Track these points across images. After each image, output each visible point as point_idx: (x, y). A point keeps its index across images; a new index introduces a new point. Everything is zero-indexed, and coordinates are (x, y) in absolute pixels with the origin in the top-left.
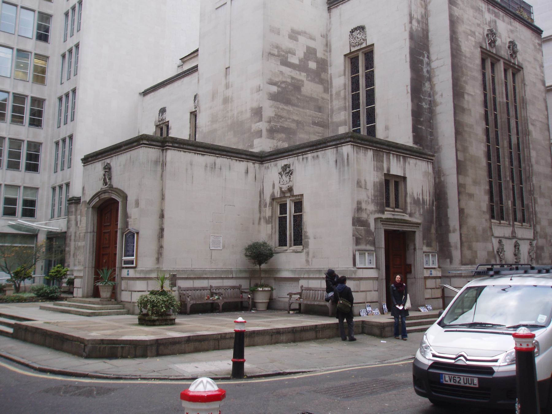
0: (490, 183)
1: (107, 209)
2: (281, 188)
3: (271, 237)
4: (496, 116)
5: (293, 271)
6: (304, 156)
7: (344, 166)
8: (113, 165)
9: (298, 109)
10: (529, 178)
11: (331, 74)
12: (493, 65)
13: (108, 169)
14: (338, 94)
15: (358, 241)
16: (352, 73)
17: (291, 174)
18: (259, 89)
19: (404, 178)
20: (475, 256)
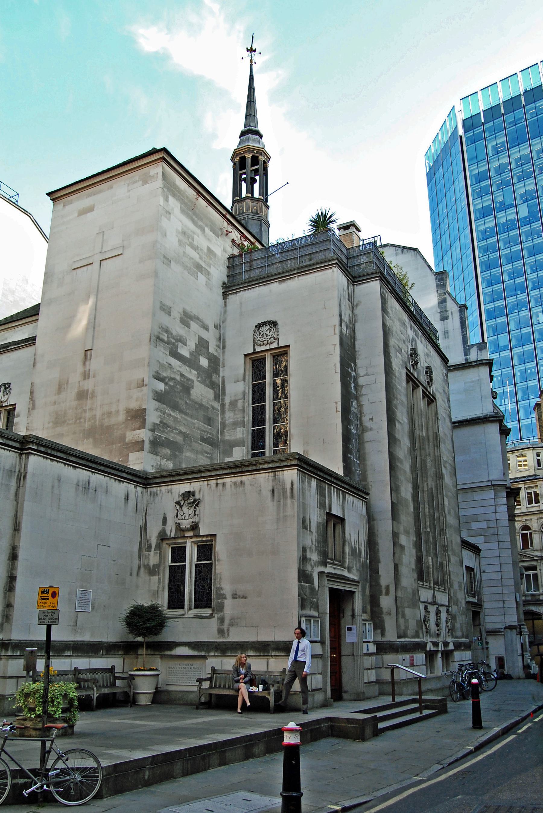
2: (178, 525)
6: (219, 481)
7: (285, 498)
9: (186, 417)
11: (223, 377)
14: (233, 404)
17: (197, 505)
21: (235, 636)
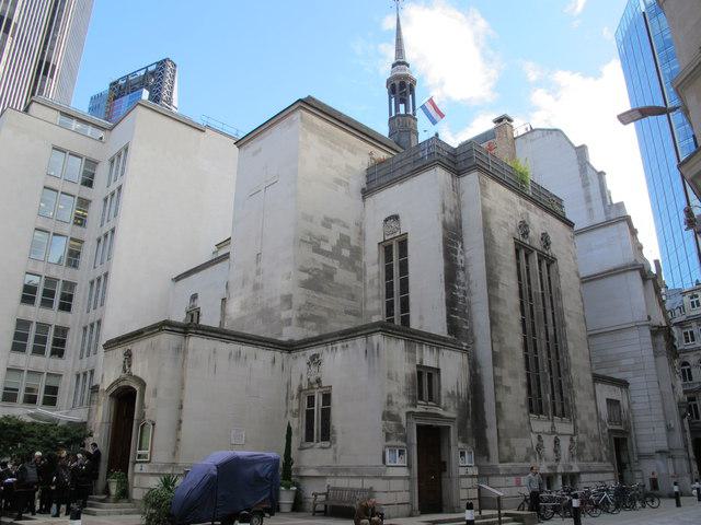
0: (528, 375)
1: (125, 399)
4: (531, 306)
5: (318, 469)
10: (567, 371)
12: (526, 256)
13: (128, 355)
14: (372, 282)
15: (388, 436)
16: (387, 261)
19: (438, 370)
20: (513, 454)
21: (344, 461)
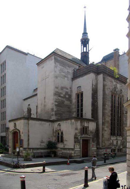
0: (112, 127)
3: (55, 140)
8: (16, 123)
13: (15, 124)
14: (74, 104)
15: (75, 142)
18: (53, 104)
21: (66, 147)
